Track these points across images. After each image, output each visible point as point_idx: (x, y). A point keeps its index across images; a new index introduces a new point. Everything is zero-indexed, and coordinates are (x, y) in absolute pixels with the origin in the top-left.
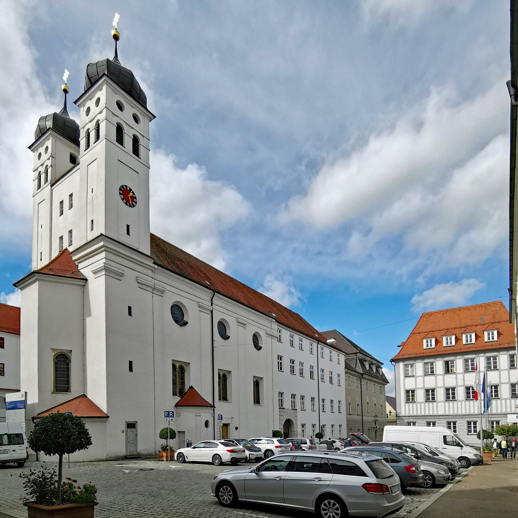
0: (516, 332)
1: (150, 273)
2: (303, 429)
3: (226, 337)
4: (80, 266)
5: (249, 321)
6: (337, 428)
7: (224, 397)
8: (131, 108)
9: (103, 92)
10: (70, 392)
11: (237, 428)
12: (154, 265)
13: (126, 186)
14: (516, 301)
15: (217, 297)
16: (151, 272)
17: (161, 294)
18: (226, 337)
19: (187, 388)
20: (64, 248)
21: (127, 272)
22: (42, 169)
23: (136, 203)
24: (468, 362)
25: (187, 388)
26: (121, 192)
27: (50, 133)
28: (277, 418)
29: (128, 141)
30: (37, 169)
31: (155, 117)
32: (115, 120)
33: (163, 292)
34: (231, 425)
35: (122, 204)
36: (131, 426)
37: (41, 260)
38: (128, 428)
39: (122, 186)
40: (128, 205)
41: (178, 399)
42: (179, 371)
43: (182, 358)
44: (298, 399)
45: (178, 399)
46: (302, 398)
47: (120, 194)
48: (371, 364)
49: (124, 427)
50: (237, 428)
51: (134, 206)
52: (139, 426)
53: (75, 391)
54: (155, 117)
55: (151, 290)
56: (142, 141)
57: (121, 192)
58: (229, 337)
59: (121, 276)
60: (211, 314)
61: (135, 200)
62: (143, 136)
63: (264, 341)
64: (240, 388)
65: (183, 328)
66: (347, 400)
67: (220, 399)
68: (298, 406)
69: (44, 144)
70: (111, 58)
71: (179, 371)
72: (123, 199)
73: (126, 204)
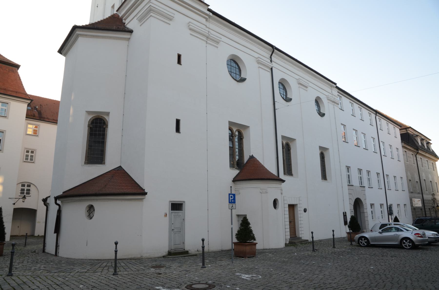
1: (203, 21)
2: (372, 210)
3: (288, 100)
4: (126, 22)
5: (311, 84)
6: (402, 206)
7: (289, 171)
10: (104, 163)
11: (305, 210)
14: (409, 190)
15: (276, 54)
16: (204, 20)
18: (288, 100)
19: (246, 159)
25: (246, 159)
28: (347, 197)
33: (218, 42)
34: (299, 206)
36: (177, 207)
38: (172, 210)
41: (236, 172)
42: (237, 135)
44: (364, 173)
45: (236, 172)
46: (368, 172)
48: (422, 140)
49: (167, 208)
50: (305, 210)
52: (187, 207)
53: (112, 161)
55: (205, 39)
58: (291, 100)
59: (171, 20)
60: (270, 71)
63: (327, 107)
64: (305, 159)
65: (240, 84)
66: (407, 177)
67: (284, 174)
68: (366, 184)
71: (237, 135)
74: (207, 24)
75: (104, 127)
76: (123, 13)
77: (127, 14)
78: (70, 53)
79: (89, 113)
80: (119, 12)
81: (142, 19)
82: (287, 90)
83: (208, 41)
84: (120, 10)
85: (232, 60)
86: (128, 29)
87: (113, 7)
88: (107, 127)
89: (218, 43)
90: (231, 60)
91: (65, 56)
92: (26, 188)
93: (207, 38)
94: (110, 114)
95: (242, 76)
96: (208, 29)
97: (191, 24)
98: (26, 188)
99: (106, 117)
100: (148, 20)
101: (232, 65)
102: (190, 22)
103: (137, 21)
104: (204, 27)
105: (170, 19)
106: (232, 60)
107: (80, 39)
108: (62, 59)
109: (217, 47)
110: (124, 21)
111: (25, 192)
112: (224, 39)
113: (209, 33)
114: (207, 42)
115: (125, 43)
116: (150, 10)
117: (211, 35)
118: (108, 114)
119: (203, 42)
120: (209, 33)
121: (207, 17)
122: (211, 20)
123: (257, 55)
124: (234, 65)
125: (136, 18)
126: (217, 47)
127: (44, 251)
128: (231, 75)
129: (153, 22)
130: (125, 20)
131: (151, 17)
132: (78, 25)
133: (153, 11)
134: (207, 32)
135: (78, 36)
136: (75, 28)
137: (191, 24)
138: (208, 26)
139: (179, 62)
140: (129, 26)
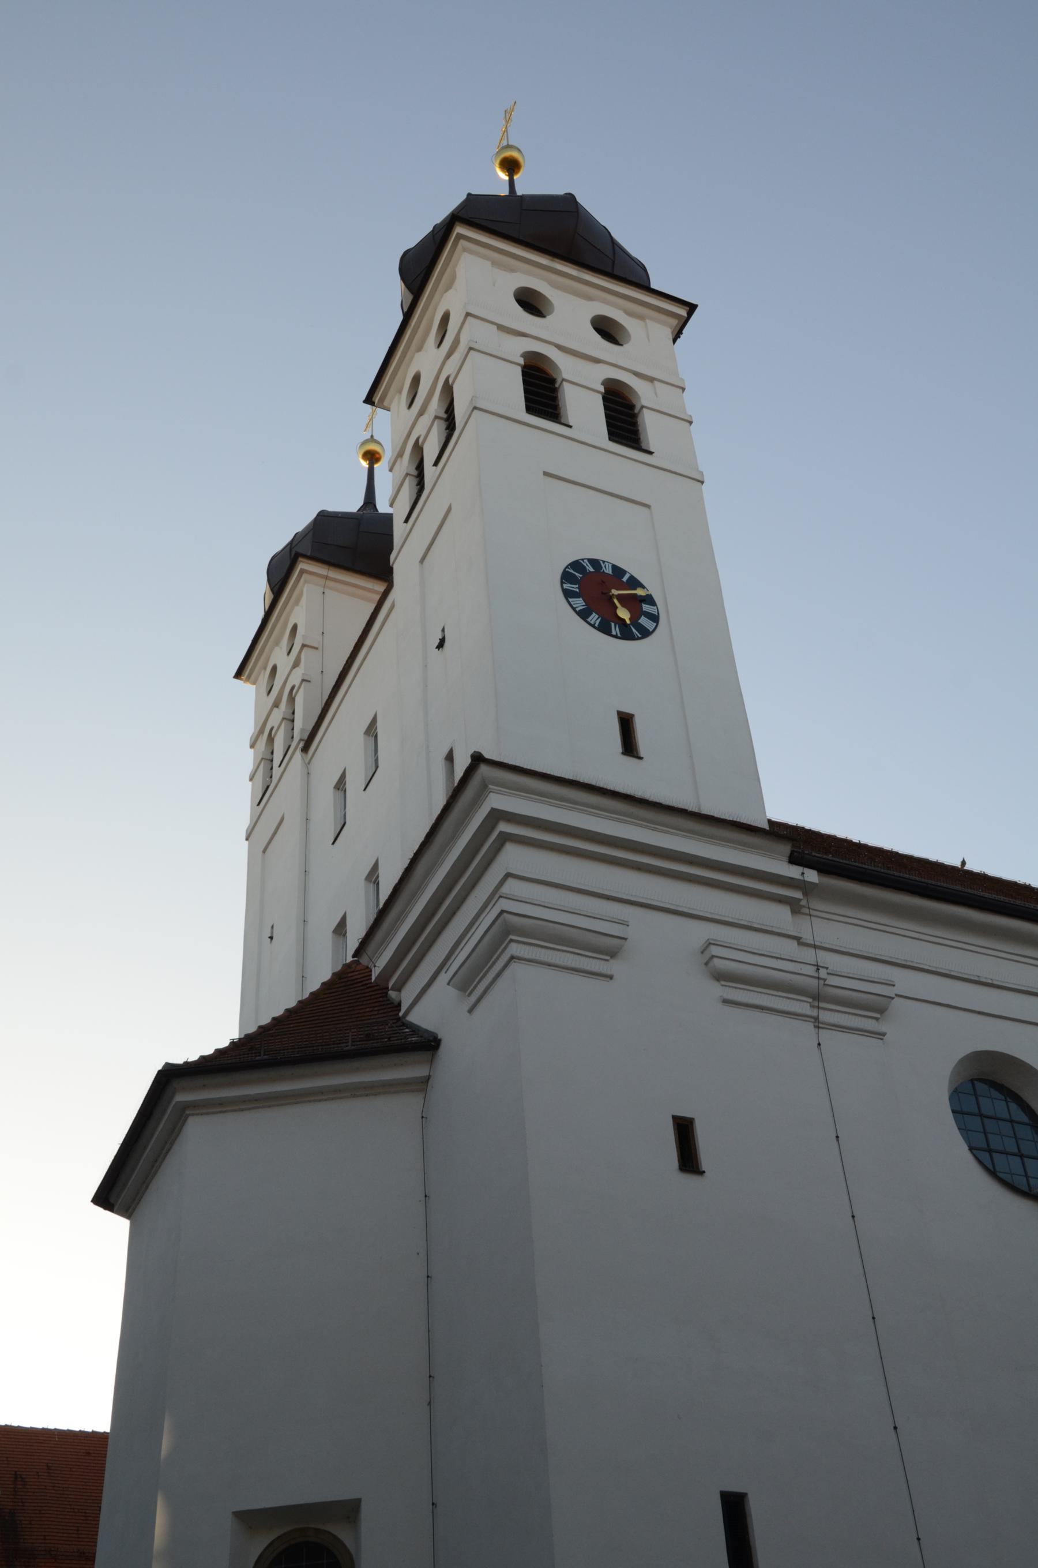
0: (634, 630)
1: (779, 916)
4: (406, 997)
8: (575, 304)
9: (481, 278)
12: (794, 872)
13: (595, 562)
17: (870, 1025)
23: (655, 618)
26: (575, 588)
29: (584, 408)
31: (692, 308)
32: (516, 349)
33: (877, 1008)
35: (585, 636)
37: (271, 938)
39: (576, 565)
40: (615, 630)
43: (734, 1486)
47: (568, 594)
51: (645, 633)
54: (692, 308)
55: (802, 1007)
56: (644, 394)
57: (575, 588)
59: (612, 954)
61: (646, 607)
62: (652, 380)
72: (583, 615)
73: (604, 628)
74: (803, 927)
75: (609, 570)
77: (402, 960)
78: (152, 1201)
79: (250, 1520)
81: (474, 979)
83: (825, 1016)
84: (371, 948)
85: (980, 1080)
86: (415, 1030)
87: (341, 929)
89: (882, 1011)
90: (972, 1081)
91: (128, 1217)
93: (817, 997)
96: (809, 955)
97: (715, 950)
99: (343, 1534)
100: (500, 982)
102: (709, 944)
103: (452, 991)
104: (790, 948)
106: (980, 1080)
107: (191, 1121)
108: (116, 1228)
109: (880, 1035)
110: (392, 994)
112: (905, 981)
115: (409, 1104)
116: (505, 931)
118: (349, 1511)
120: (823, 973)
121: (798, 895)
122: (817, 904)
124: (1000, 1107)
125: (444, 977)
126: (880, 1035)
127: (475, 408)
128: (993, 1173)
129: (529, 986)
130: (399, 988)
131: (515, 966)
132: (179, 1059)
133: (522, 932)
134: (810, 970)
135: (183, 1113)
136: (169, 1077)
137: (715, 950)
138: (807, 937)
139: (688, 1159)
140: (423, 1016)
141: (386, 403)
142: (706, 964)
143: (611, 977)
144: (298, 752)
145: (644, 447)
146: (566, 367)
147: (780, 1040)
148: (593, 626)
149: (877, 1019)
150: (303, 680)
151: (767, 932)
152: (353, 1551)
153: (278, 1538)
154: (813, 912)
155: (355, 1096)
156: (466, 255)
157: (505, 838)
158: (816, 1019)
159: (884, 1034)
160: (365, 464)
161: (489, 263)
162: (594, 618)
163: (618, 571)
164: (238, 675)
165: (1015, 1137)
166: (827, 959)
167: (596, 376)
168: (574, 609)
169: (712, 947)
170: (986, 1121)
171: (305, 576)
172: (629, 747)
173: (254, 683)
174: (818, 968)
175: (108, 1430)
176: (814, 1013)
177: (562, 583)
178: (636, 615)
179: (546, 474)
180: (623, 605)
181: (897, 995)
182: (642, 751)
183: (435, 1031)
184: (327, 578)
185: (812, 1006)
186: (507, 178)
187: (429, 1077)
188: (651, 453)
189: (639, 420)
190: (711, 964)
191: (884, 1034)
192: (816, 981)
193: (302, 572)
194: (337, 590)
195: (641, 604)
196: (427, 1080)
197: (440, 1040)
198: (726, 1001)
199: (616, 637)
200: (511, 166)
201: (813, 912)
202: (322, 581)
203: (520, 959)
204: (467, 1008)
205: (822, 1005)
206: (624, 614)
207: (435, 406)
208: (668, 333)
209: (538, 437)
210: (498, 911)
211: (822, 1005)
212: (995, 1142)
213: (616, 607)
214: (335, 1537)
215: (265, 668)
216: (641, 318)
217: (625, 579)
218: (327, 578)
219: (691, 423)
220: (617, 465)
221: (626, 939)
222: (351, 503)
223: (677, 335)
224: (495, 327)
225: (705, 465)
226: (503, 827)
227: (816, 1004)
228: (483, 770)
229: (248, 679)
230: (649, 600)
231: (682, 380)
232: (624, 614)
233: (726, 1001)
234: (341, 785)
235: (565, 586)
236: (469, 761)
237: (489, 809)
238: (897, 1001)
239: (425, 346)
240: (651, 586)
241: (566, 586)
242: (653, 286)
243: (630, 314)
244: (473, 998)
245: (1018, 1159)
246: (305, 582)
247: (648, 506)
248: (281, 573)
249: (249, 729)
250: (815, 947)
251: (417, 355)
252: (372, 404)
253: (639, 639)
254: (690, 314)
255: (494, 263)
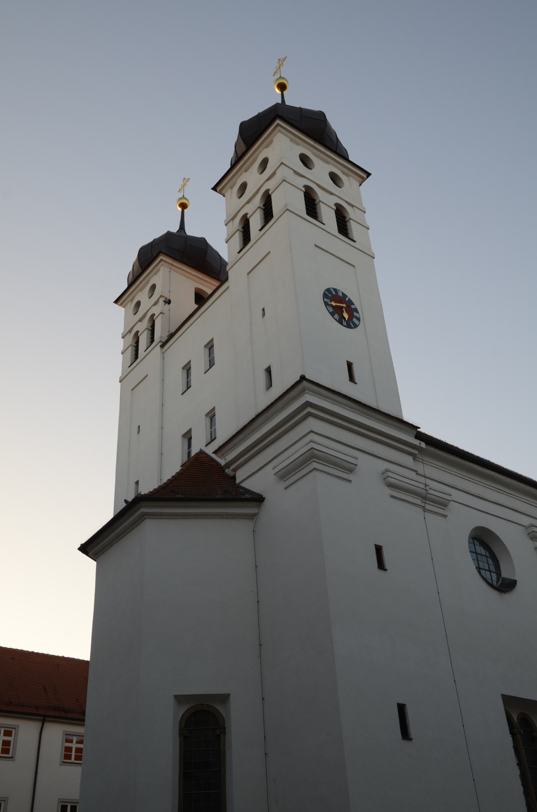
1: (408, 460)
4: (240, 476)
8: (322, 168)
9: (282, 146)
13: (335, 290)
20: (195, 451)
21: (364, 462)
22: (144, 326)
23: (359, 319)
24: (71, 751)
27: (161, 260)
30: (130, 331)
31: (369, 175)
32: (301, 182)
33: (444, 504)
35: (332, 323)
39: (328, 290)
54: (369, 175)
55: (418, 501)
56: (351, 213)
59: (351, 471)
61: (355, 314)
69: (148, 282)
70: (280, 102)
75: (341, 295)
76: (230, 456)
79: (180, 699)
80: (220, 454)
82: (494, 551)
83: (428, 507)
84: (224, 451)
86: (247, 491)
88: (224, 733)
92: (74, 745)
93: (425, 498)
94: (232, 698)
95: (505, 574)
96: (422, 480)
97: (389, 474)
98: (74, 745)
99: (221, 709)
101: (478, 551)
104: (413, 475)
105: (350, 468)
109: (445, 516)
111: (73, 754)
112: (456, 495)
113: (428, 488)
114: (424, 509)
117: (431, 492)
119: (417, 509)
120: (428, 488)
121: (416, 452)
123: (526, 521)
126: (445, 516)
127: (287, 210)
131: (315, 472)
134: (423, 486)
137: (389, 474)
138: (421, 471)
139: (381, 565)
141: (223, 192)
142: (384, 479)
143: (350, 481)
144: (158, 347)
145: (350, 236)
146: (321, 195)
147: (410, 514)
148: (336, 320)
149: (443, 509)
150: (161, 313)
151: (409, 469)
152: (224, 715)
153: (191, 707)
154: (424, 462)
155: (222, 518)
156: (279, 134)
157: (309, 414)
158: (424, 507)
159: (447, 516)
160: (180, 209)
161: (289, 139)
162: (336, 316)
163: (345, 296)
164: (116, 302)
165: (488, 563)
166: (429, 482)
167: (332, 201)
168: (329, 311)
169: (388, 472)
170: (478, 556)
171: (162, 263)
172: (352, 378)
173: (124, 307)
174: (426, 485)
175: (80, 649)
176: (423, 505)
177: (324, 298)
178: (351, 316)
179: (316, 246)
180: (347, 312)
181: (453, 501)
182: (357, 379)
183: (261, 494)
184: (172, 265)
185: (422, 502)
186: (280, 93)
187: (258, 513)
188: (355, 241)
189: (348, 224)
190: (387, 479)
191: (447, 516)
192: (425, 491)
193: (161, 260)
194: (176, 271)
195: (352, 310)
196: (256, 514)
197: (264, 498)
198: (392, 497)
199: (345, 326)
200: (282, 87)
201: (424, 462)
202: (170, 266)
203: (318, 470)
204: (284, 487)
205: (427, 502)
206: (346, 316)
207: (258, 201)
208: (358, 184)
209: (306, 227)
210: (310, 448)
211: (427, 502)
212: (481, 566)
213: (343, 312)
214: (218, 710)
215: (132, 301)
216: (347, 175)
217: (347, 299)
218: (172, 265)
219: (368, 229)
220: (338, 244)
221: (357, 465)
222: (175, 228)
223: (360, 185)
224: (292, 171)
225: (375, 249)
226: (309, 409)
227: (424, 501)
228: (305, 383)
229: (121, 305)
230: (356, 310)
231: (364, 208)
232: (346, 316)
233: (392, 497)
234: (187, 368)
235: (325, 300)
236: (298, 378)
237: (305, 401)
238: (451, 502)
239: (250, 170)
240: (357, 304)
241: (325, 300)
242: (350, 159)
243: (343, 173)
244: (288, 483)
245: (489, 573)
246: (162, 265)
247: (354, 266)
248: (147, 257)
249: (121, 329)
250: (425, 477)
251: (244, 173)
252: (216, 191)
253: (353, 328)
254: (367, 177)
255: (291, 140)
